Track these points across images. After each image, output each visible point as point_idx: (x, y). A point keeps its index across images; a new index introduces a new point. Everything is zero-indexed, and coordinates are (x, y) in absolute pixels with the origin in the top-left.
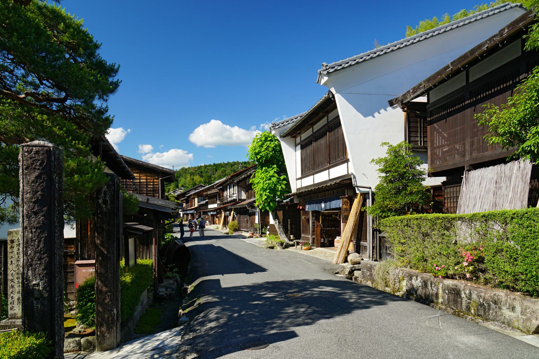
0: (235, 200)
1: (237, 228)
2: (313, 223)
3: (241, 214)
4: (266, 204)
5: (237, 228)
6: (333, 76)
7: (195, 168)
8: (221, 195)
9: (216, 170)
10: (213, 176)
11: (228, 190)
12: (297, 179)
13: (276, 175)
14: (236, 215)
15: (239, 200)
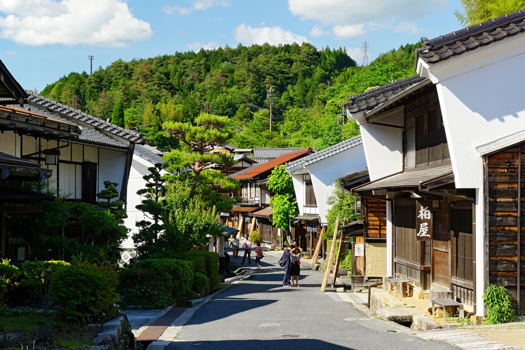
0: (257, 205)
1: (259, 239)
2: (313, 239)
3: (263, 223)
4: (281, 224)
5: (259, 239)
6: (308, 167)
7: (151, 61)
8: (239, 192)
9: (208, 70)
10: (197, 85)
11: (249, 188)
12: (304, 206)
13: (288, 202)
14: (259, 223)
15: (262, 205)
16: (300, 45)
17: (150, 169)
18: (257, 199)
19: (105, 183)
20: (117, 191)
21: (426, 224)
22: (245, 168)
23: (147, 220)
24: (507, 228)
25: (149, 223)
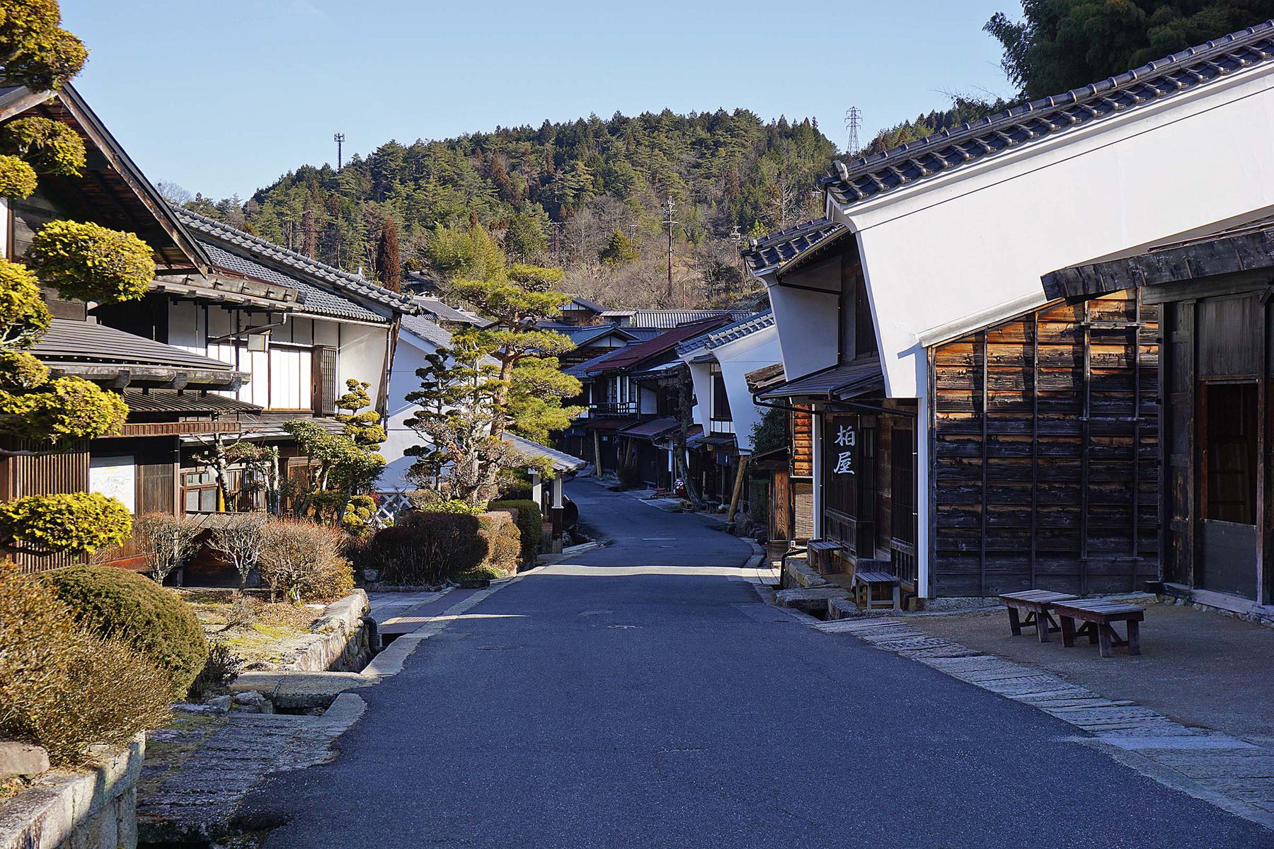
16: (731, 114)
17: (428, 358)
18: (632, 405)
19: (348, 383)
20: (368, 396)
21: (848, 453)
22: (615, 348)
23: (422, 444)
24: (965, 461)
25: (425, 450)
